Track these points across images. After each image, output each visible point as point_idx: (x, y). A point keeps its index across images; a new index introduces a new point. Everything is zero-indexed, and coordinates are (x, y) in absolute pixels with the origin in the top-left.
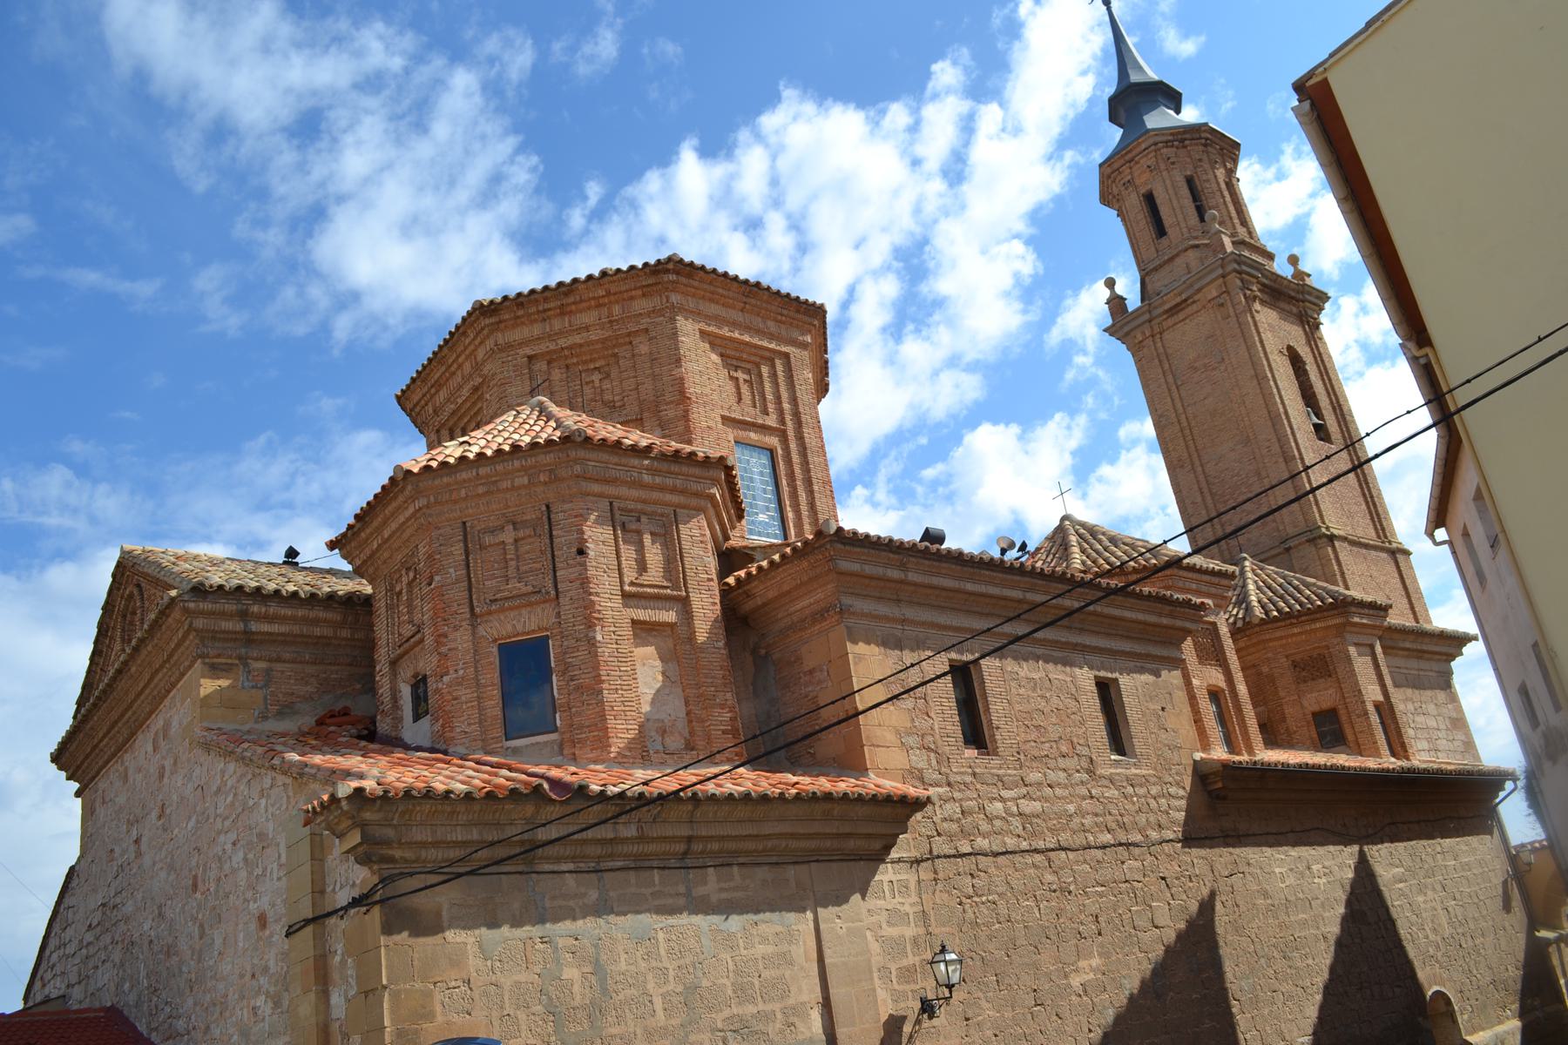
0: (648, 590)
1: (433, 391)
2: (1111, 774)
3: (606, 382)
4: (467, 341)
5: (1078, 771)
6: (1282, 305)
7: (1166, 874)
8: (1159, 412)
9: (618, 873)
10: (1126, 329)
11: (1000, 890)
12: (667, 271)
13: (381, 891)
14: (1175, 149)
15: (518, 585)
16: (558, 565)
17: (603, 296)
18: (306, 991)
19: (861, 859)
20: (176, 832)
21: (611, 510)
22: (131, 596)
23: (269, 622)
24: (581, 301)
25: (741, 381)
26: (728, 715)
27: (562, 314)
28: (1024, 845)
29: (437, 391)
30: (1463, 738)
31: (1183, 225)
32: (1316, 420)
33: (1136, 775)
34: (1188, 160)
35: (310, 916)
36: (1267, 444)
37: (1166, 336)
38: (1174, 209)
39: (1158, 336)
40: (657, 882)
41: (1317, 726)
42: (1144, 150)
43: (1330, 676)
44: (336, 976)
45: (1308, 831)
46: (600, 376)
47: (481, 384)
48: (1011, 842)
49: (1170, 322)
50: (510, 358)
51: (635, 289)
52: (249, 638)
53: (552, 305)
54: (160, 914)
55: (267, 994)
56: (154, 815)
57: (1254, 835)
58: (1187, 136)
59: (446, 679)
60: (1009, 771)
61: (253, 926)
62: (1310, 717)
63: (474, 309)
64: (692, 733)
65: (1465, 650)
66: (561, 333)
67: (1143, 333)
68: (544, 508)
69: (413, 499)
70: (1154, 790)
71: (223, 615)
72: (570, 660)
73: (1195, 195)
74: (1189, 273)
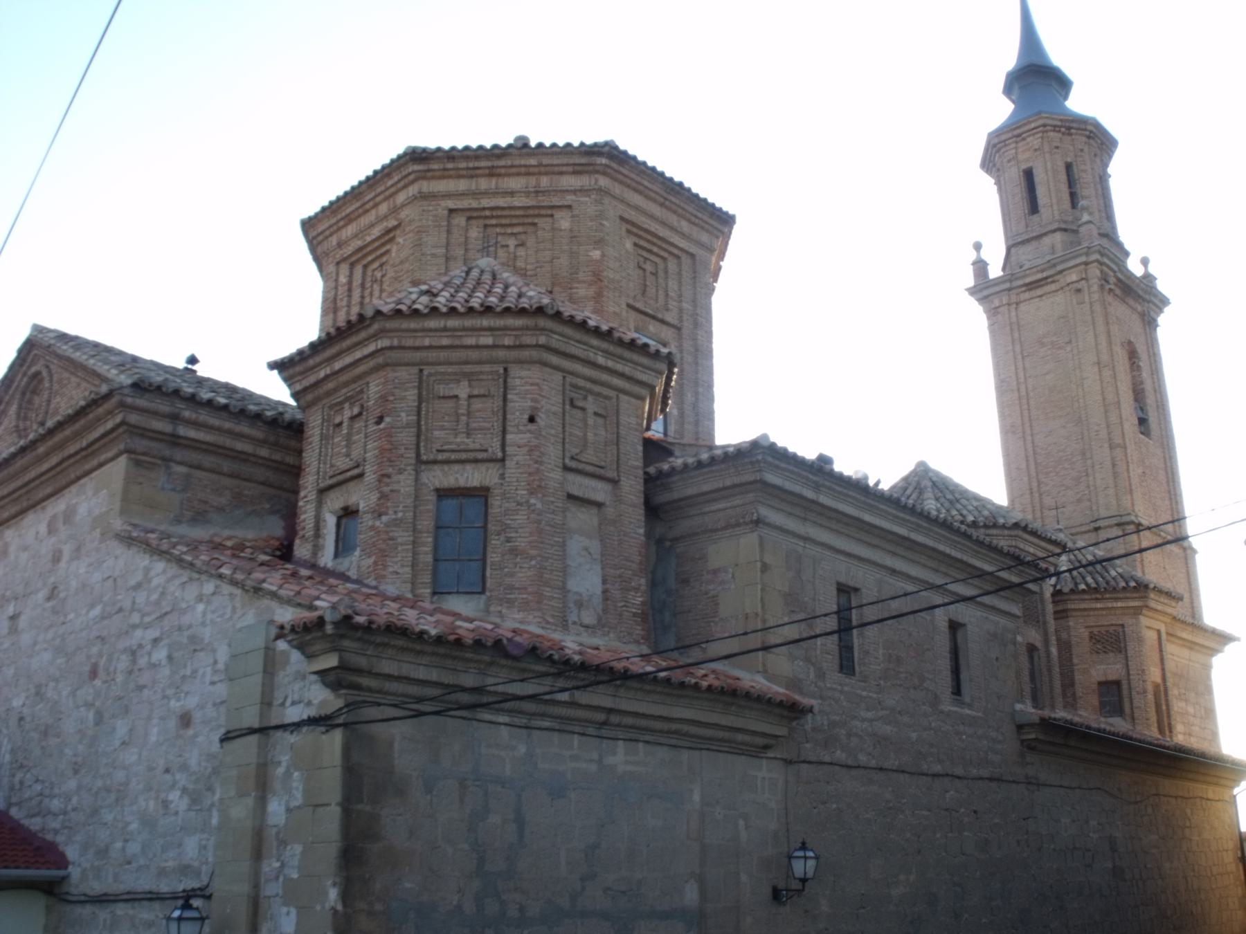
1: (341, 223)
2: (950, 711)
3: (521, 249)
9: (545, 732)
13: (344, 716)
14: (1060, 135)
15: (466, 440)
16: (509, 429)
18: (242, 794)
19: (743, 754)
20: (71, 616)
21: (564, 385)
22: (38, 374)
25: (648, 274)
26: (640, 599)
27: (491, 175)
29: (346, 225)
31: (1055, 207)
33: (968, 715)
34: (1071, 148)
35: (256, 725)
36: (1096, 428)
37: (1023, 307)
38: (1049, 191)
39: (1014, 306)
41: (1101, 695)
42: (1033, 129)
43: (1120, 652)
44: (277, 785)
45: (1092, 789)
46: (516, 243)
49: (1027, 295)
50: (431, 208)
52: (174, 440)
54: (37, 694)
55: (184, 790)
56: (41, 595)
57: (1051, 786)
58: (1074, 125)
59: (384, 518)
60: (870, 694)
61: (172, 723)
62: (1095, 687)
64: (605, 611)
66: (485, 194)
69: (375, 337)
71: (155, 414)
72: (508, 522)
73: (1071, 182)
74: (1053, 253)
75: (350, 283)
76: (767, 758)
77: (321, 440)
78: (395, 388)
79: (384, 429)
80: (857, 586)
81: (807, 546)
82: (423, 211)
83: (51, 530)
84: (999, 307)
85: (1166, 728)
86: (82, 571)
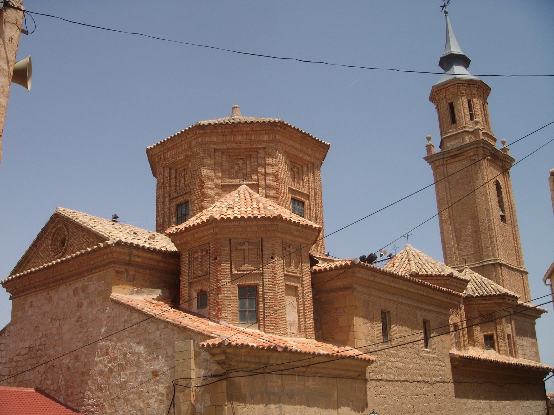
0: (292, 274)
2: (424, 355)
4: (188, 137)
5: (414, 354)
6: (497, 162)
7: (436, 393)
8: (440, 197)
10: (432, 160)
11: (388, 393)
12: (277, 126)
17: (249, 131)
19: (351, 378)
23: (137, 257)
24: (240, 131)
25: (295, 173)
28: (396, 378)
30: (535, 350)
32: (501, 213)
33: (431, 357)
37: (449, 166)
40: (297, 380)
47: (191, 155)
48: (392, 377)
49: (452, 161)
50: (207, 148)
51: (263, 130)
53: (228, 130)
56: (73, 320)
57: (464, 382)
58: (471, 83)
63: (196, 126)
65: (542, 315)
67: (439, 163)
68: (260, 239)
70: (436, 363)
75: (170, 176)
76: (359, 379)
77: (189, 263)
78: (221, 246)
79: (217, 262)
80: (389, 310)
81: (371, 297)
82: (203, 149)
83: (75, 293)
84: (439, 166)
85: (514, 353)
86: (95, 312)
